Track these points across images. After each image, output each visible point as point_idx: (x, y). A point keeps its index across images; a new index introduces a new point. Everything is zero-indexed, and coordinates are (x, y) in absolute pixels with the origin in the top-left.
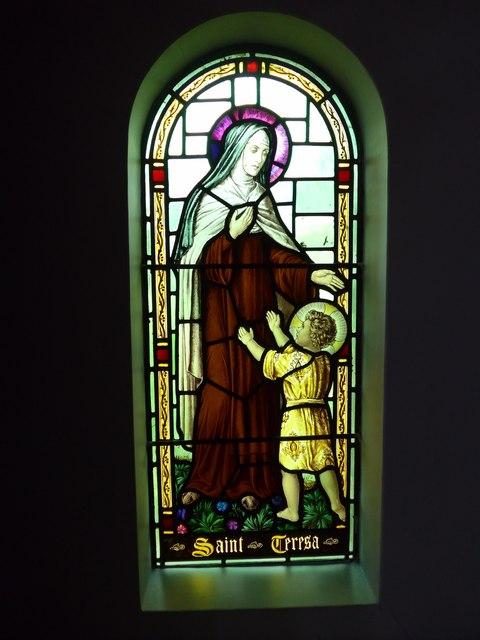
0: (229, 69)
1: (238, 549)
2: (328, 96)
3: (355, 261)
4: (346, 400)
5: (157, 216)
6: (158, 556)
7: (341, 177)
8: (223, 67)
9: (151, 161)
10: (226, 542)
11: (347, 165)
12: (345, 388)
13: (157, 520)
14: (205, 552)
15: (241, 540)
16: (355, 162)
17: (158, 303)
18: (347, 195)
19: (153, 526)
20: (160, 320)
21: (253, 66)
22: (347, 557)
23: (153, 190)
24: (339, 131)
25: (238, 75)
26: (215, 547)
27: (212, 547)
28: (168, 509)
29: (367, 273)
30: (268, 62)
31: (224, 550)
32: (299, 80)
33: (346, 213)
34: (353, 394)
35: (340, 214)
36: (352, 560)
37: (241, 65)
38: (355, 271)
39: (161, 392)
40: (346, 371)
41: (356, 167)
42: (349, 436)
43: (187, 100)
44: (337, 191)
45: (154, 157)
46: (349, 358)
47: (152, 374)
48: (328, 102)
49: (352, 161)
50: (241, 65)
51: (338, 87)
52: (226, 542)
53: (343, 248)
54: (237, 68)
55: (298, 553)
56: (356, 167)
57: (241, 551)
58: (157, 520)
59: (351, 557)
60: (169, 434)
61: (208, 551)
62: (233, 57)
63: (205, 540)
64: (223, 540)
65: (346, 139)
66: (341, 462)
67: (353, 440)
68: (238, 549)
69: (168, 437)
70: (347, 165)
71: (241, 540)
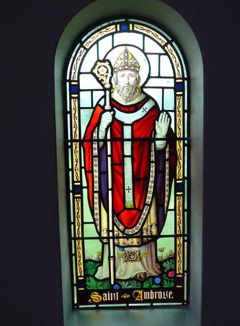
0: (112, 29)
1: (110, 298)
2: (169, 42)
3: (186, 136)
4: (182, 117)
5: (73, 112)
6: (76, 302)
7: (178, 87)
8: (107, 28)
9: (70, 81)
10: (109, 294)
11: (181, 81)
12: (181, 208)
13: (75, 282)
14: (98, 299)
15: (117, 293)
16: (186, 79)
17: (74, 160)
18: (182, 97)
19: (72, 285)
20: (76, 170)
21: (124, 28)
22: (183, 304)
23: (71, 98)
24: (176, 61)
25: (117, 32)
26: (102, 296)
27: (100, 297)
28: (81, 276)
29: (193, 143)
30: (133, 23)
31: (107, 298)
32: (153, 34)
33: (181, 109)
34: (186, 213)
35: (177, 110)
36: (185, 305)
37: (118, 26)
38: (186, 238)
39: (77, 211)
40: (181, 99)
41: (186, 82)
42: (184, 139)
43: (88, 47)
44: (176, 95)
45: (72, 79)
46: (183, 191)
47: (186, 76)
48: (169, 46)
49: (183, 78)
50: (118, 26)
51: (174, 38)
52: (109, 294)
53: (180, 227)
54: (116, 27)
55: (157, 300)
56: (186, 82)
57: (117, 299)
58: (75, 282)
59: (185, 303)
60: (81, 234)
61: (98, 299)
62: (115, 21)
63: (97, 293)
64: (107, 293)
65: (180, 65)
66: (180, 153)
67: (186, 142)
68: (110, 298)
69: (80, 236)
70: (181, 81)
71: (117, 293)
